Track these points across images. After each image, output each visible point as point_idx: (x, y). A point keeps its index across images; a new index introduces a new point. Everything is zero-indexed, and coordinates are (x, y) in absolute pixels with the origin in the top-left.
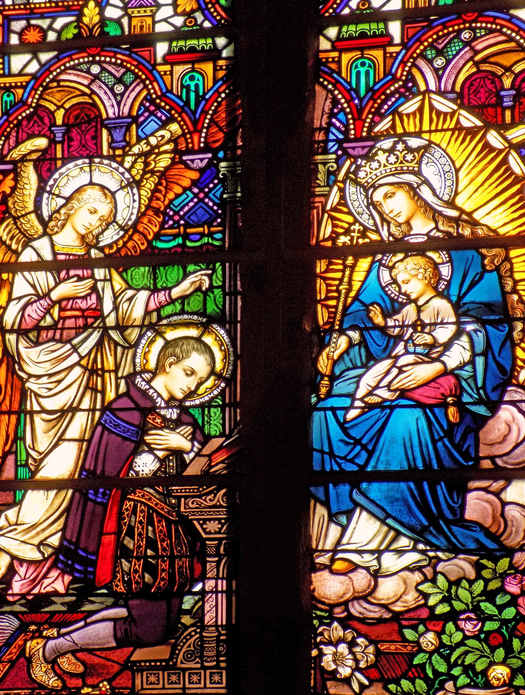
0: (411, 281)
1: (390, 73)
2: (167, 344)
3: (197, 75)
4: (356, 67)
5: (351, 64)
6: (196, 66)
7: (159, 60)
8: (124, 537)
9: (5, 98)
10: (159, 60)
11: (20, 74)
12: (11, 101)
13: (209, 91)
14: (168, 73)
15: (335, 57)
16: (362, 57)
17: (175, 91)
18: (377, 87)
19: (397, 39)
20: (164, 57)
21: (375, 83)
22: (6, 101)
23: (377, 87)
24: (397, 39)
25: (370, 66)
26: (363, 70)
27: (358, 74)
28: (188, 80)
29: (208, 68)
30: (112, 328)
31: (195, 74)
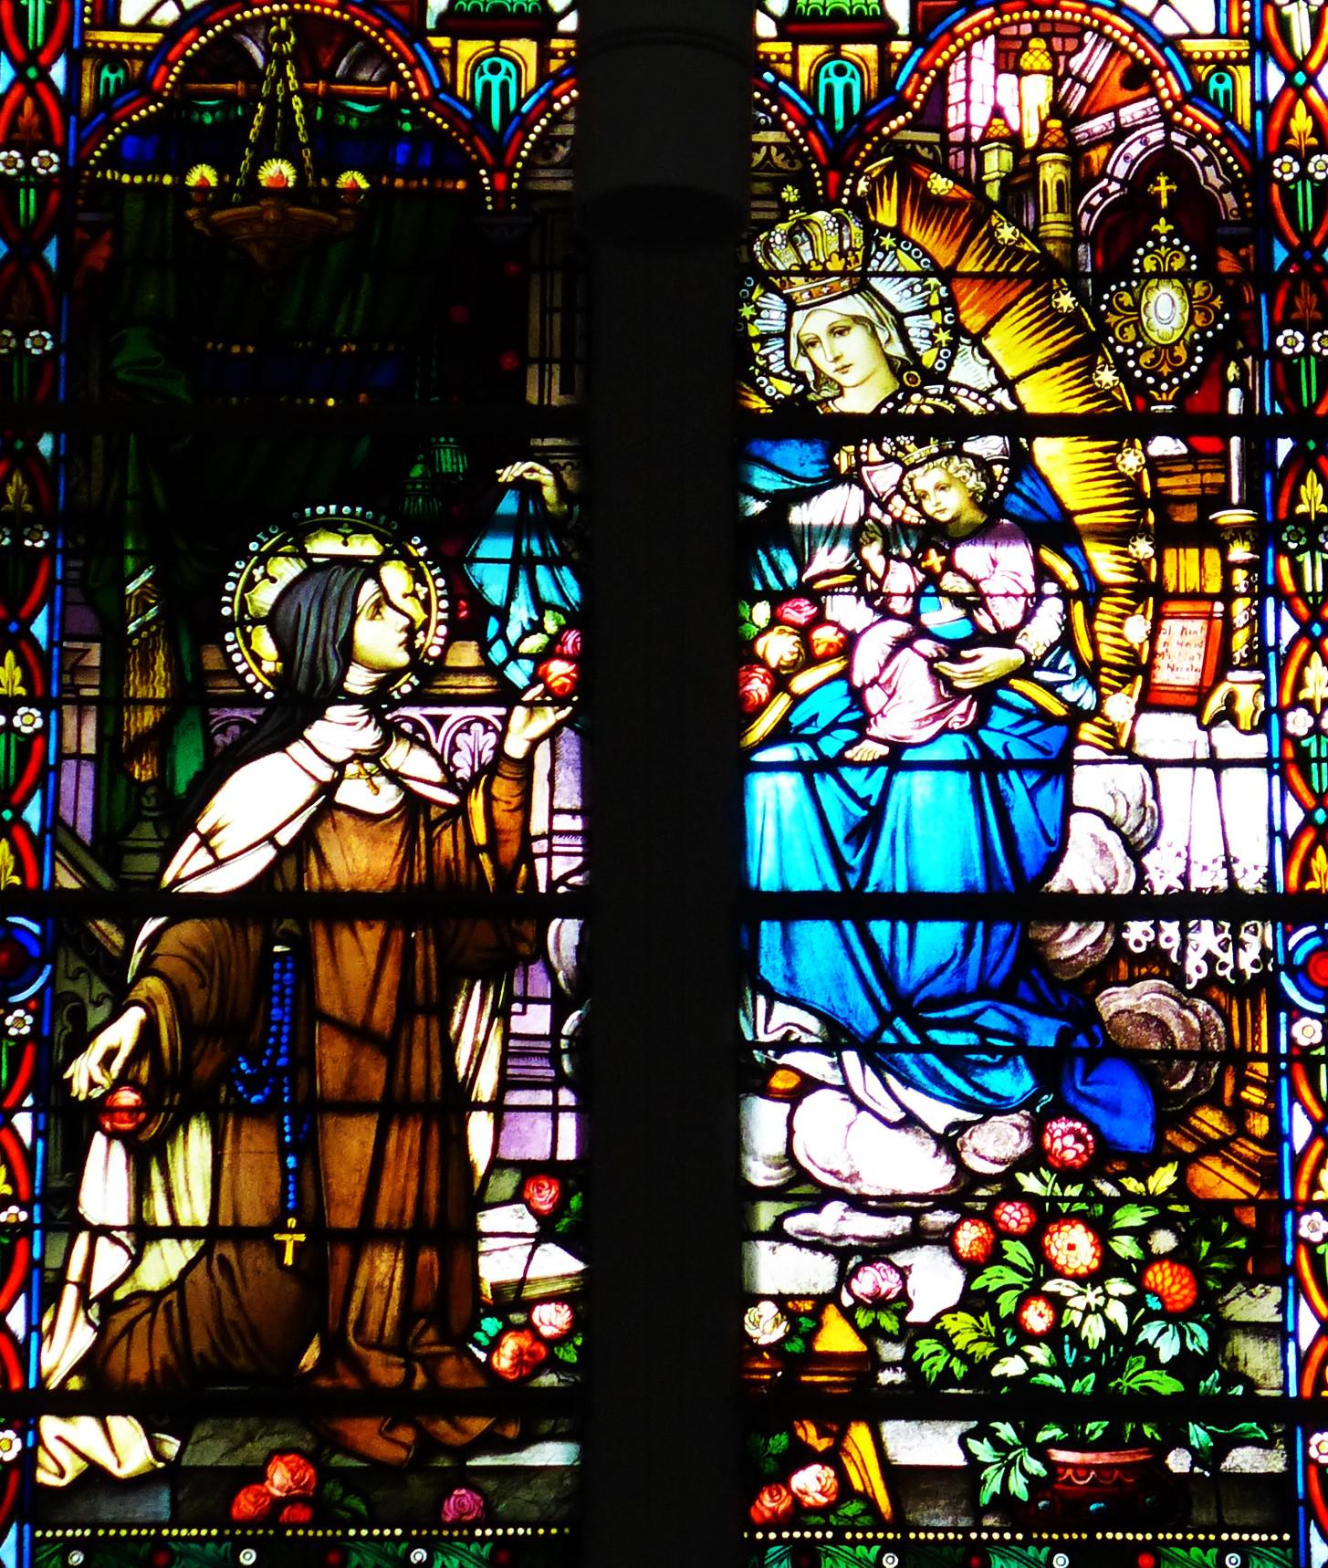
0: (953, 489)
1: (893, 91)
2: (314, 568)
3: (505, 64)
4: (852, 76)
5: (818, 67)
6: (504, 43)
7: (431, 23)
8: (978, 1087)
9: (105, 73)
10: (431, 23)
11: (144, 25)
12: (118, 80)
13: (529, 95)
14: (787, 57)
15: (570, 50)
16: (497, 53)
17: (460, 91)
18: (525, 108)
19: (904, 29)
20: (442, 18)
21: (520, 102)
22: (107, 81)
23: (525, 108)
24: (904, 29)
25: (508, 73)
26: (496, 81)
27: (487, 86)
28: (831, 72)
29: (525, 49)
30: (380, 561)
31: (497, 60)
